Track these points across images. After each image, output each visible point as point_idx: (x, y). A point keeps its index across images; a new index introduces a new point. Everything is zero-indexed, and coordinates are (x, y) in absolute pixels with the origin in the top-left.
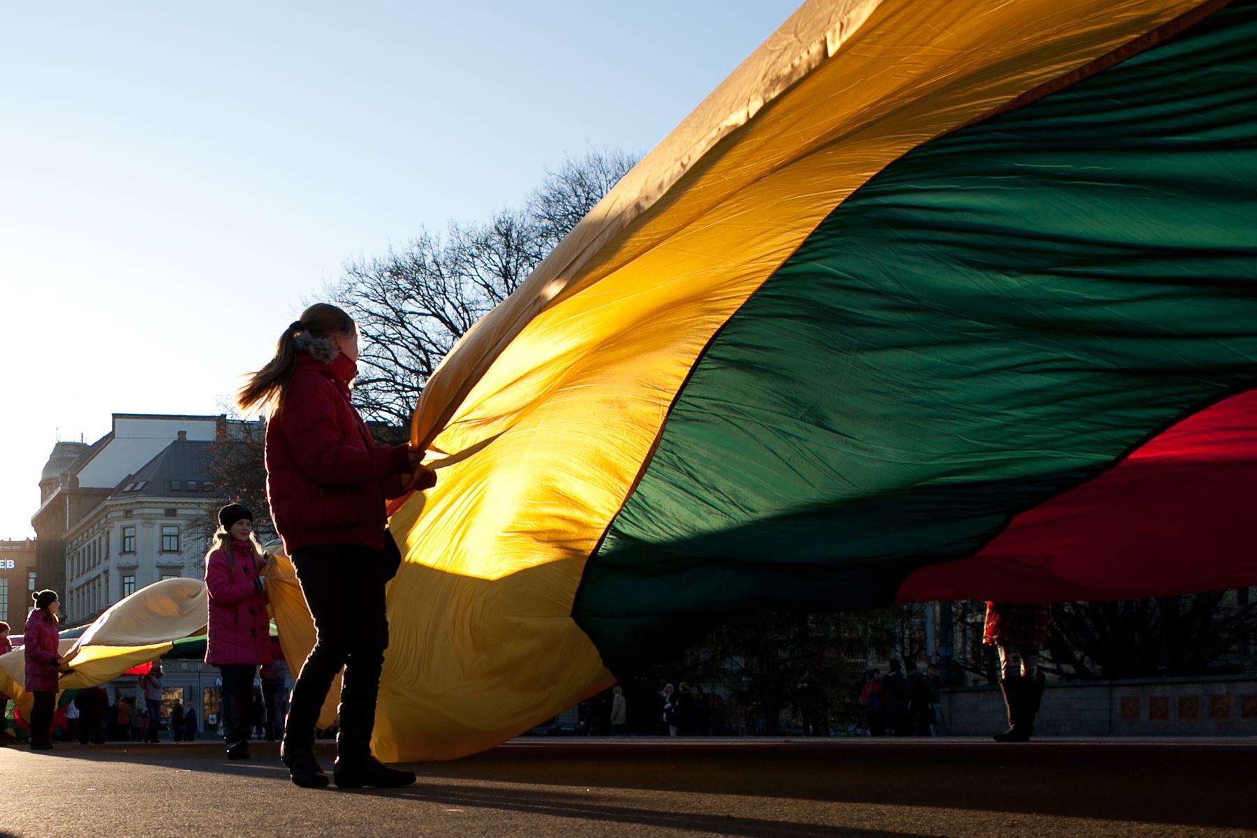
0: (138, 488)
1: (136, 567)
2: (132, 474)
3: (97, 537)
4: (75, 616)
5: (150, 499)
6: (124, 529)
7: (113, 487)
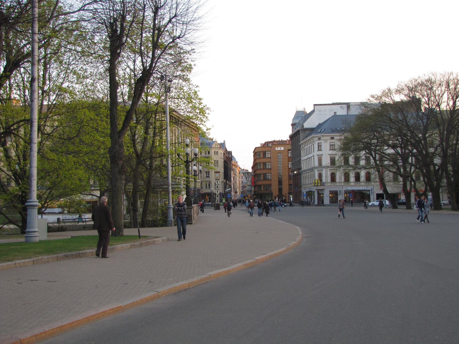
0: (322, 131)
2: (321, 123)
7: (315, 127)
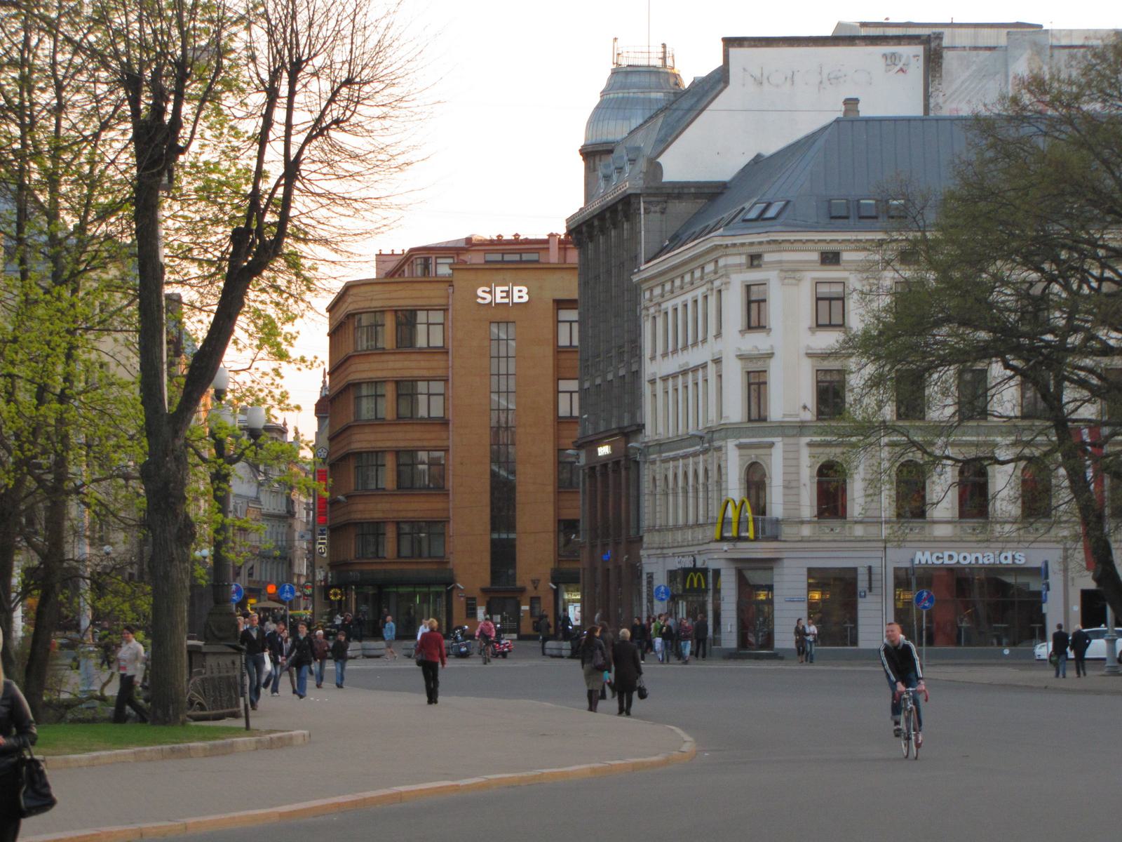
0: (771, 213)
1: (770, 355)
3: (699, 293)
4: (661, 429)
5: (792, 237)
6: (748, 287)
